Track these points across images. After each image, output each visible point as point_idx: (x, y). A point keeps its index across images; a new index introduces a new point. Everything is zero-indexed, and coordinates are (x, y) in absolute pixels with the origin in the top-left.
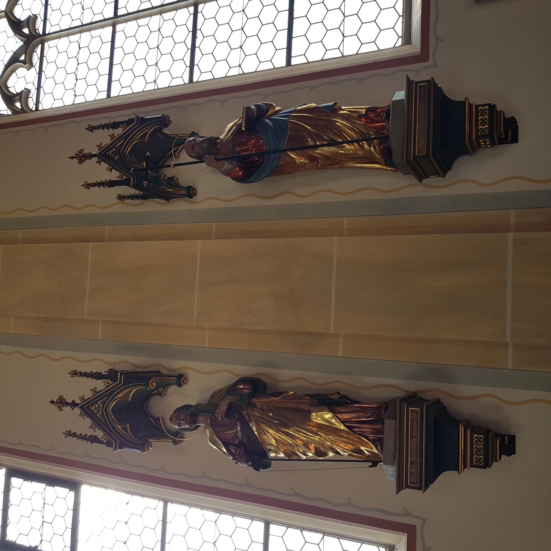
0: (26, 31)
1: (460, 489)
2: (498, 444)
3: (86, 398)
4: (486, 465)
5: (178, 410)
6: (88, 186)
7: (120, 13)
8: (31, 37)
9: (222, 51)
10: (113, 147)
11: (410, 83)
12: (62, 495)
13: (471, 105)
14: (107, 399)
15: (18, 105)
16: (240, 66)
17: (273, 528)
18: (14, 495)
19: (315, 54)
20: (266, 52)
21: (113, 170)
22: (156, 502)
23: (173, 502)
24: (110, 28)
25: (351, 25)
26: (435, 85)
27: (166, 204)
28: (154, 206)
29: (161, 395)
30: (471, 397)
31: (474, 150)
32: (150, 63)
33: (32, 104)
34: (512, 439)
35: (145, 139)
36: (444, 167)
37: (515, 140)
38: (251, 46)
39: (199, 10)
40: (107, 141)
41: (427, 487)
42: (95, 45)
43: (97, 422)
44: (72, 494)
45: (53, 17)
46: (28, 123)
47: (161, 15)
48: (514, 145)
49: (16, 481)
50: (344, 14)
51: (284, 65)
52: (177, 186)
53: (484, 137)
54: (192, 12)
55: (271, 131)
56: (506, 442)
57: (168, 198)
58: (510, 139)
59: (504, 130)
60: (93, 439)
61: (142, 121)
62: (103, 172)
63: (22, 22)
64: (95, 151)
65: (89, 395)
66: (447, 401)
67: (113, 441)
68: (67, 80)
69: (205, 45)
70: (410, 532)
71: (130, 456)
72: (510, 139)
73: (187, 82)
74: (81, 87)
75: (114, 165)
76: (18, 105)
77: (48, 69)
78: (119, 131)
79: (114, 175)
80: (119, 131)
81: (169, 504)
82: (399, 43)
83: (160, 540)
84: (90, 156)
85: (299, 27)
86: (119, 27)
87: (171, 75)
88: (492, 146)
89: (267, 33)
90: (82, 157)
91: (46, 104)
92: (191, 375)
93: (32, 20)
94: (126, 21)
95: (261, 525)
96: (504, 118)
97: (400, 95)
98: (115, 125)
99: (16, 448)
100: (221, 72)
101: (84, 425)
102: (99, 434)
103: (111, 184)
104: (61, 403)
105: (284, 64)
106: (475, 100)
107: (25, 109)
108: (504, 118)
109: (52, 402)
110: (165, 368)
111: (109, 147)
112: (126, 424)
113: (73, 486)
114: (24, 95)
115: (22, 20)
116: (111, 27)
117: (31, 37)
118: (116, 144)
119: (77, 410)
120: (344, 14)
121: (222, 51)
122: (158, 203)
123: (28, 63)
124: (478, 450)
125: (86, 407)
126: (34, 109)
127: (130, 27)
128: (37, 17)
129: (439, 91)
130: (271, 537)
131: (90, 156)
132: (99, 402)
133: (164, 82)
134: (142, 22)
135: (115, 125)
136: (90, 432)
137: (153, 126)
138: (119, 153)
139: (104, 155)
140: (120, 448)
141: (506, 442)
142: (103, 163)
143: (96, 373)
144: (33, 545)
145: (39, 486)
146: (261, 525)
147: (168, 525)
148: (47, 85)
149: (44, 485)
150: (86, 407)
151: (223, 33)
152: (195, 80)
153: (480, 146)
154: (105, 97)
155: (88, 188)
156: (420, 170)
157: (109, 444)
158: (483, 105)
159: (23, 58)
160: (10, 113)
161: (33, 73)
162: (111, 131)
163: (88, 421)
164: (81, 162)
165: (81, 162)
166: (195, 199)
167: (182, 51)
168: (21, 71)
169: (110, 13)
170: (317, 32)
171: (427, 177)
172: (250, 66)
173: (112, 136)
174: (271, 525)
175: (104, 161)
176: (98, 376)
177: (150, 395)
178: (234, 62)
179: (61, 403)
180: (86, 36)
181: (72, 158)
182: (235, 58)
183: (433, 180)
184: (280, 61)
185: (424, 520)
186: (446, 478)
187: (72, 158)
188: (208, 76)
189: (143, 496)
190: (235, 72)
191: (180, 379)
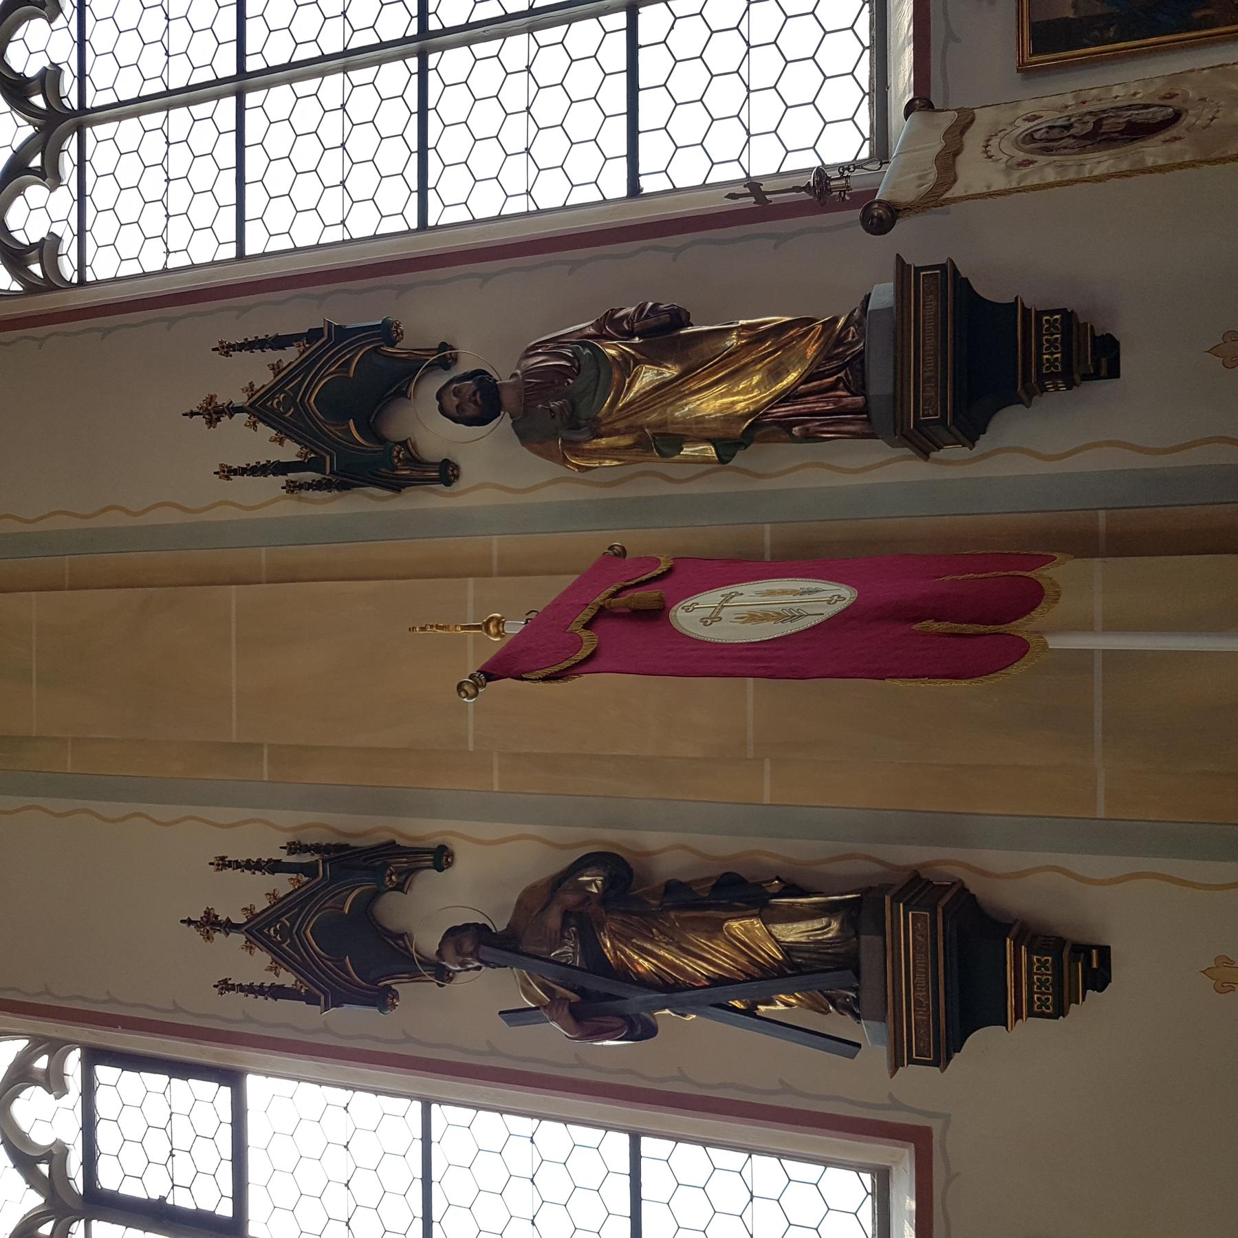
0: (38, 100)
1: (1010, 1061)
2: (1078, 967)
3: (258, 911)
4: (1060, 1011)
5: (452, 932)
6: (228, 472)
7: (253, 64)
8: (58, 120)
9: (486, 159)
10: (281, 391)
11: (902, 267)
12: (211, 1098)
13: (1026, 311)
14: (299, 914)
15: (36, 269)
16: (528, 193)
17: (647, 1144)
18: (104, 1102)
19: (689, 172)
20: (584, 163)
21: (287, 441)
22: (405, 1102)
23: (441, 1102)
24: (231, 101)
25: (764, 111)
26: (956, 272)
27: (393, 497)
28: (363, 503)
29: (401, 890)
30: (1022, 874)
31: (1030, 394)
32: (328, 183)
33: (68, 270)
34: (1105, 952)
35: (348, 372)
36: (969, 428)
37: (1114, 372)
38: (549, 148)
39: (431, 64)
40: (265, 378)
41: (949, 1059)
42: (203, 137)
43: (281, 959)
44: (226, 1092)
45: (100, 71)
46: (59, 312)
47: (345, 73)
48: (1106, 386)
49: (104, 1073)
50: (748, 87)
51: (624, 193)
52: (414, 460)
53: (1053, 376)
54: (415, 69)
55: (600, 328)
56: (1095, 966)
57: (397, 486)
58: (1103, 372)
59: (1087, 353)
60: (277, 992)
61: (341, 333)
62: (262, 444)
63: (29, 80)
64: (241, 399)
65: (262, 904)
66: (975, 886)
67: (318, 992)
68: (140, 212)
69: (448, 144)
70: (920, 1140)
71: (353, 1020)
72: (1103, 372)
73: (414, 225)
74: (179, 232)
75: (285, 430)
76: (36, 269)
77: (101, 193)
78: (290, 355)
79: (290, 452)
80: (290, 355)
81: (435, 1108)
82: (865, 154)
83: (434, 1185)
84: (232, 410)
85: (652, 108)
86: (252, 99)
87: (377, 209)
88: (1069, 388)
89: (584, 121)
90: (213, 413)
91: (102, 267)
92: (461, 850)
93: (50, 76)
94: (268, 86)
95: (624, 1139)
96: (1094, 337)
97: (883, 295)
98: (279, 342)
99: (101, 1009)
100: (486, 205)
101: (256, 966)
102: (287, 979)
103: (280, 468)
104: (210, 924)
105: (623, 192)
106: (1033, 301)
107: (53, 282)
108: (1094, 337)
109: (189, 922)
110: (401, 835)
111: (271, 391)
112: (335, 956)
113: (232, 1078)
114: (48, 248)
115: (28, 75)
116: (234, 98)
117: (58, 120)
118: (287, 384)
119: (239, 939)
120: (748, 87)
121: (486, 159)
122: (371, 497)
123: (50, 176)
124: (1042, 983)
125: (258, 929)
126: (75, 280)
127: (279, 98)
128: (61, 70)
129: (963, 285)
130: (644, 1162)
131: (232, 410)
132: (283, 919)
133: (363, 225)
134: (304, 87)
135: (279, 342)
136: (269, 979)
137: (362, 346)
138: (294, 404)
139: (260, 408)
140: (337, 1004)
141: (1095, 966)
142: (260, 425)
143: (270, 860)
144: (155, 1196)
145: (157, 1081)
146: (621, 1141)
147: (435, 1148)
148: (101, 228)
149: (166, 1078)
150: (258, 929)
151: (486, 118)
152: (431, 223)
153: (1044, 390)
154: (233, 255)
155: (228, 478)
156: (922, 442)
157: (311, 999)
158: (1052, 312)
159: (36, 162)
160: (17, 287)
161: (63, 200)
162: (273, 356)
163: (263, 958)
164: (211, 423)
165: (211, 423)
166: (455, 487)
167: (398, 156)
168: (36, 193)
169: (228, 68)
170: (689, 124)
171: (939, 448)
172: (551, 194)
173: (277, 368)
174: (643, 1139)
175: (264, 422)
176: (274, 867)
177: (377, 894)
178: (516, 183)
179: (210, 924)
180: (179, 116)
181: (192, 414)
182: (516, 174)
183: (949, 452)
184: (616, 187)
185: (947, 1118)
186: (983, 1040)
187: (192, 414)
188: (461, 215)
189: (377, 1092)
190: (518, 206)
191: (441, 857)
